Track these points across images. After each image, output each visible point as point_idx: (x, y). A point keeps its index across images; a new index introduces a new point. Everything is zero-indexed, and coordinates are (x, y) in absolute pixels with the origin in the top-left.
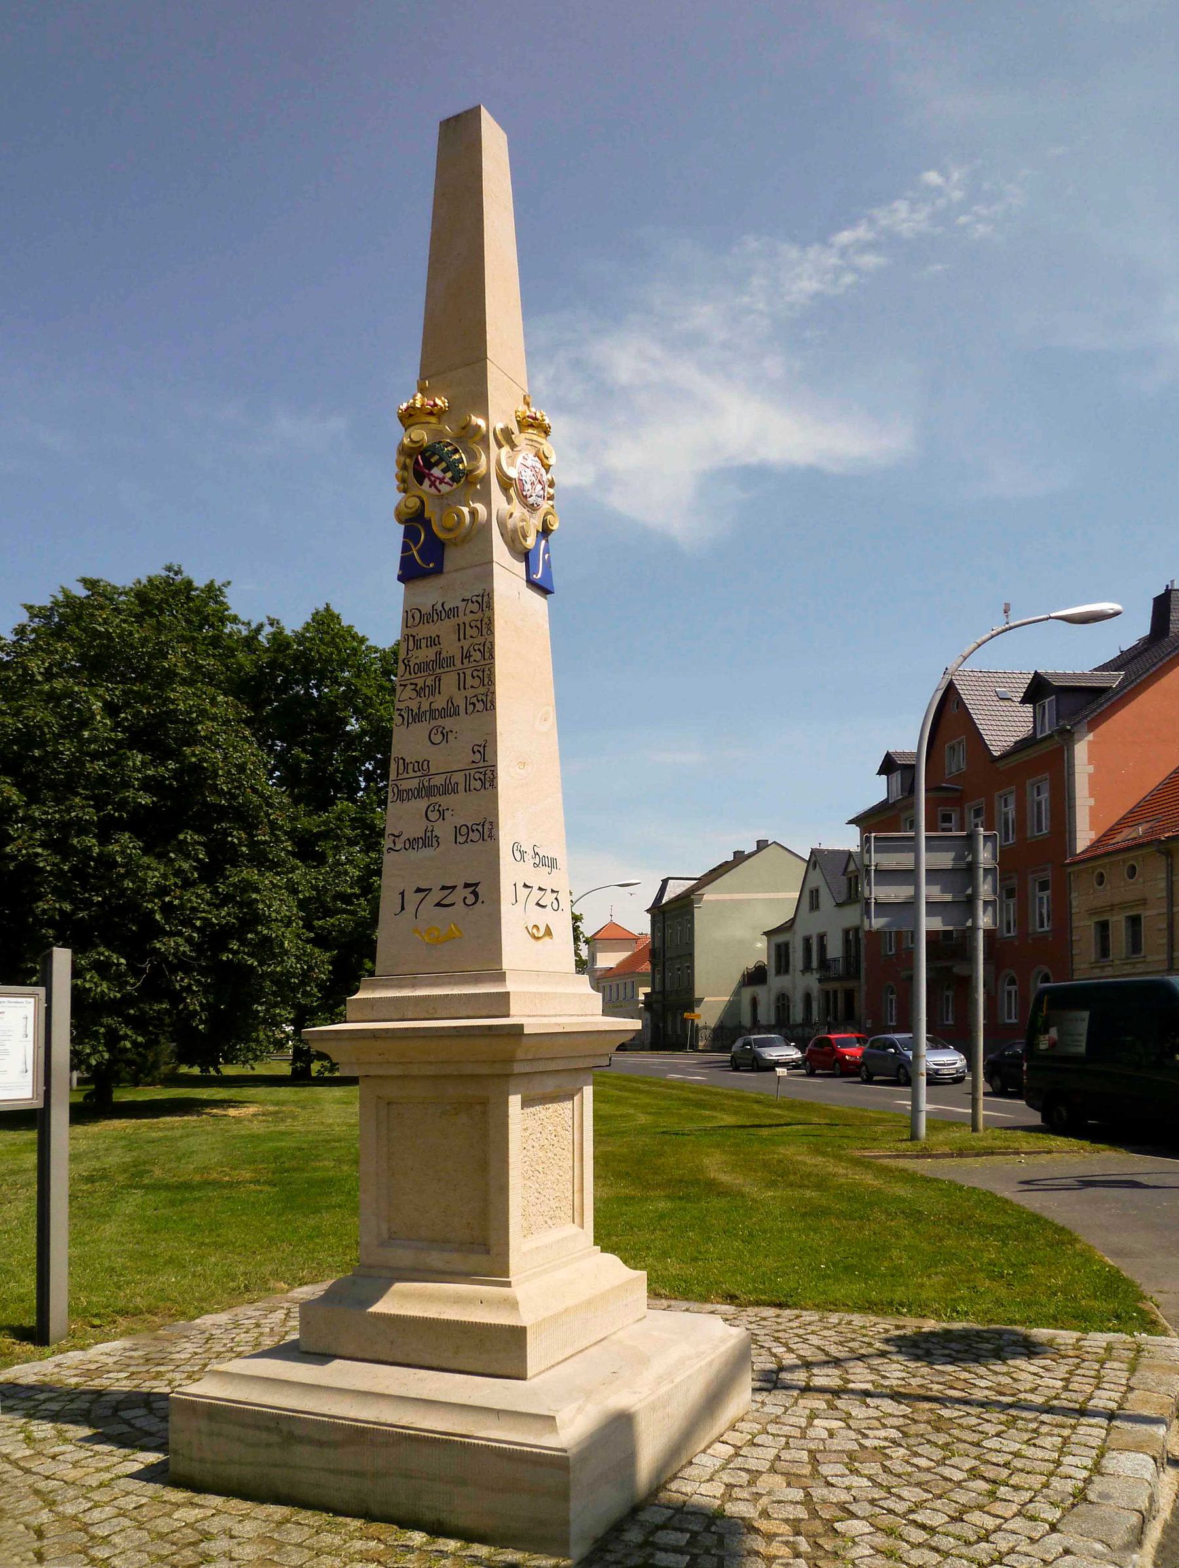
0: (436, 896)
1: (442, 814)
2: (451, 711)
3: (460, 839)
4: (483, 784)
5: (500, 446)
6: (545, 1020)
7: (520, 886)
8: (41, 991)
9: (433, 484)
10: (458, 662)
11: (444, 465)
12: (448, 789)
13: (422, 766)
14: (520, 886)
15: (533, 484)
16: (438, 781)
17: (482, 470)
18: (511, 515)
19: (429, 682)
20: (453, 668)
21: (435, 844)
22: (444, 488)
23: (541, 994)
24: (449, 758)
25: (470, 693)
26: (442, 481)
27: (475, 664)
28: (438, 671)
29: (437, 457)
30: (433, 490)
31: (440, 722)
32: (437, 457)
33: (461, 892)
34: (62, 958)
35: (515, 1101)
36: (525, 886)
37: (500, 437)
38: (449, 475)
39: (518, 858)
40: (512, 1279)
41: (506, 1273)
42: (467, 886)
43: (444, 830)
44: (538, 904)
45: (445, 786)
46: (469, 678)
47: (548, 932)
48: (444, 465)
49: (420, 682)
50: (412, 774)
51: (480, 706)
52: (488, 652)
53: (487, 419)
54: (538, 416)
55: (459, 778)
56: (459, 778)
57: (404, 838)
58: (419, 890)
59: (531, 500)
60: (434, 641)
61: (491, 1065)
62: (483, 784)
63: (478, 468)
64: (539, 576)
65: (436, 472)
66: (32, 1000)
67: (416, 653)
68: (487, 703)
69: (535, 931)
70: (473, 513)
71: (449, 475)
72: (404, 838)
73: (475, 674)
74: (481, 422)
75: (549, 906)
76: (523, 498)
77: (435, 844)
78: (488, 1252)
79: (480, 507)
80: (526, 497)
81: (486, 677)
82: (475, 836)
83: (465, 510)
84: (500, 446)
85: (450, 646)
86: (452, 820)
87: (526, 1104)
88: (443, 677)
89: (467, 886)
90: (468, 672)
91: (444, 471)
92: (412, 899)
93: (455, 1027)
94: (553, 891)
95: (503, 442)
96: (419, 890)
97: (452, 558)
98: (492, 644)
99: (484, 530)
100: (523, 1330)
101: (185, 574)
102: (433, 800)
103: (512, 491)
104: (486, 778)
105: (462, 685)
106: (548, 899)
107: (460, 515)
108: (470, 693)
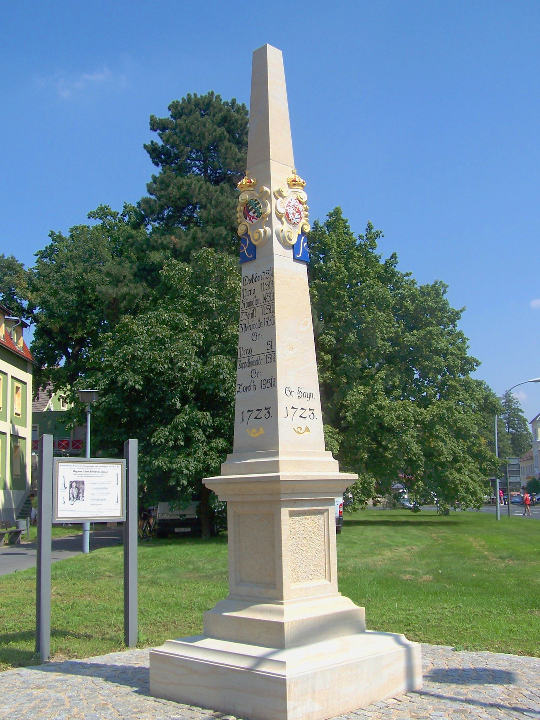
0: (255, 414)
1: (256, 374)
2: (259, 325)
3: (264, 386)
4: (271, 360)
5: (277, 199)
6: (85, 469)
7: (289, 408)
8: (124, 460)
9: (250, 219)
10: (261, 302)
11: (253, 210)
12: (259, 362)
13: (249, 351)
14: (289, 408)
15: (293, 214)
16: (255, 358)
17: (269, 211)
18: (282, 230)
19: (252, 312)
20: (260, 305)
21: (254, 389)
22: (254, 220)
23: (323, 462)
24: (259, 348)
25: (266, 316)
26: (253, 218)
27: (268, 303)
28: (255, 306)
29: (251, 207)
30: (250, 222)
31: (255, 330)
32: (251, 207)
33: (264, 412)
34: (133, 444)
35: (285, 512)
36: (293, 408)
37: (276, 195)
38: (256, 214)
39: (289, 395)
40: (284, 601)
41: (282, 598)
42: (266, 409)
43: (257, 382)
44: (301, 416)
45: (257, 361)
46: (265, 308)
47: (307, 429)
48: (253, 210)
49: (248, 311)
50: (246, 355)
51: (269, 322)
52: (271, 296)
53: (270, 188)
54: (297, 180)
55: (262, 357)
56: (262, 357)
57: (243, 386)
58: (249, 411)
59: (293, 221)
60: (253, 292)
61: (274, 496)
62: (271, 360)
63: (266, 211)
64: (300, 255)
65: (251, 213)
66: (120, 466)
67: (247, 297)
68: (271, 321)
69: (299, 429)
70: (265, 232)
71: (256, 214)
72: (243, 386)
73: (268, 307)
74: (268, 190)
75: (308, 417)
76: (289, 220)
77: (254, 389)
78: (275, 588)
79: (268, 229)
80: (290, 220)
81: (271, 308)
82: (268, 385)
83: (262, 231)
84: (277, 199)
85: (259, 295)
86: (261, 377)
87: (292, 514)
88: (257, 309)
89: (266, 409)
90: (265, 306)
91: (254, 213)
92: (246, 415)
93: (256, 477)
94: (310, 409)
95: (278, 197)
96: (249, 411)
97: (259, 252)
98: (274, 293)
99: (269, 241)
100: (283, 623)
101: (292, 177)
102: (254, 367)
103: (283, 219)
104: (271, 356)
105: (263, 313)
106: (307, 413)
107: (260, 233)
108: (266, 316)
